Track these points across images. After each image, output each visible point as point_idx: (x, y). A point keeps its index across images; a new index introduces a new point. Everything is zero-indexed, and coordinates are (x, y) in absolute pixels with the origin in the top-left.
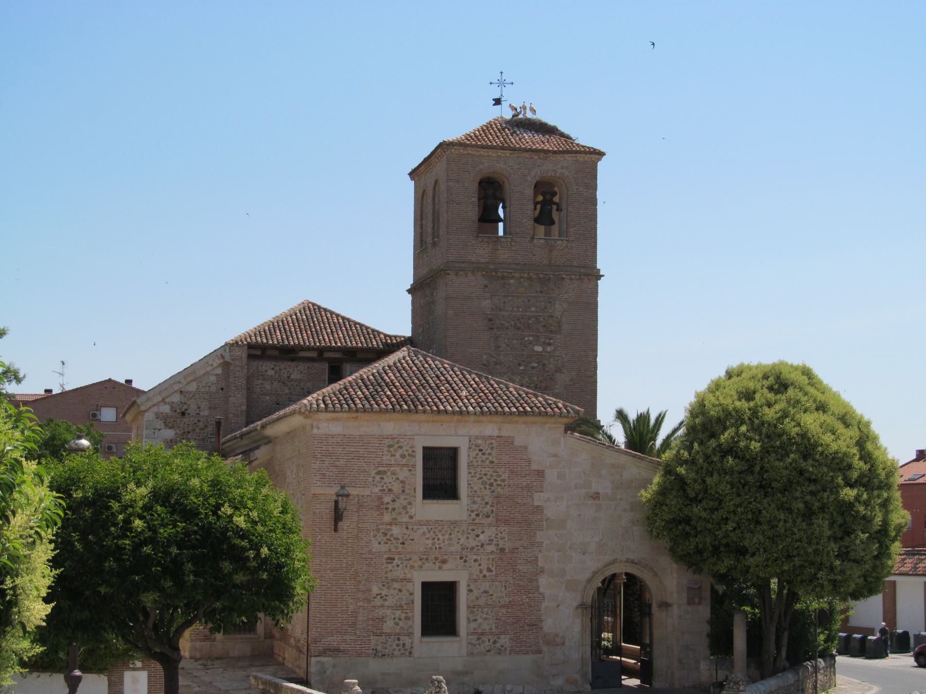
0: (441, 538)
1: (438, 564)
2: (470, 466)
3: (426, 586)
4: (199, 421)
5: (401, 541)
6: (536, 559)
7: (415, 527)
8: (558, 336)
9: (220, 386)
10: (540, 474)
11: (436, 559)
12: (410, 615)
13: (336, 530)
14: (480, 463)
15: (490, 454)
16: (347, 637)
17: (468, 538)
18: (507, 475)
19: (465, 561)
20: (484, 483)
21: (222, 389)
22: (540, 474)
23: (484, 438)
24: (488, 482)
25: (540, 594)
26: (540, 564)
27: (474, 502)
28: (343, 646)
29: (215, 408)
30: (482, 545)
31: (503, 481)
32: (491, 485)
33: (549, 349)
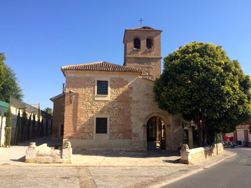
15: (117, 83)
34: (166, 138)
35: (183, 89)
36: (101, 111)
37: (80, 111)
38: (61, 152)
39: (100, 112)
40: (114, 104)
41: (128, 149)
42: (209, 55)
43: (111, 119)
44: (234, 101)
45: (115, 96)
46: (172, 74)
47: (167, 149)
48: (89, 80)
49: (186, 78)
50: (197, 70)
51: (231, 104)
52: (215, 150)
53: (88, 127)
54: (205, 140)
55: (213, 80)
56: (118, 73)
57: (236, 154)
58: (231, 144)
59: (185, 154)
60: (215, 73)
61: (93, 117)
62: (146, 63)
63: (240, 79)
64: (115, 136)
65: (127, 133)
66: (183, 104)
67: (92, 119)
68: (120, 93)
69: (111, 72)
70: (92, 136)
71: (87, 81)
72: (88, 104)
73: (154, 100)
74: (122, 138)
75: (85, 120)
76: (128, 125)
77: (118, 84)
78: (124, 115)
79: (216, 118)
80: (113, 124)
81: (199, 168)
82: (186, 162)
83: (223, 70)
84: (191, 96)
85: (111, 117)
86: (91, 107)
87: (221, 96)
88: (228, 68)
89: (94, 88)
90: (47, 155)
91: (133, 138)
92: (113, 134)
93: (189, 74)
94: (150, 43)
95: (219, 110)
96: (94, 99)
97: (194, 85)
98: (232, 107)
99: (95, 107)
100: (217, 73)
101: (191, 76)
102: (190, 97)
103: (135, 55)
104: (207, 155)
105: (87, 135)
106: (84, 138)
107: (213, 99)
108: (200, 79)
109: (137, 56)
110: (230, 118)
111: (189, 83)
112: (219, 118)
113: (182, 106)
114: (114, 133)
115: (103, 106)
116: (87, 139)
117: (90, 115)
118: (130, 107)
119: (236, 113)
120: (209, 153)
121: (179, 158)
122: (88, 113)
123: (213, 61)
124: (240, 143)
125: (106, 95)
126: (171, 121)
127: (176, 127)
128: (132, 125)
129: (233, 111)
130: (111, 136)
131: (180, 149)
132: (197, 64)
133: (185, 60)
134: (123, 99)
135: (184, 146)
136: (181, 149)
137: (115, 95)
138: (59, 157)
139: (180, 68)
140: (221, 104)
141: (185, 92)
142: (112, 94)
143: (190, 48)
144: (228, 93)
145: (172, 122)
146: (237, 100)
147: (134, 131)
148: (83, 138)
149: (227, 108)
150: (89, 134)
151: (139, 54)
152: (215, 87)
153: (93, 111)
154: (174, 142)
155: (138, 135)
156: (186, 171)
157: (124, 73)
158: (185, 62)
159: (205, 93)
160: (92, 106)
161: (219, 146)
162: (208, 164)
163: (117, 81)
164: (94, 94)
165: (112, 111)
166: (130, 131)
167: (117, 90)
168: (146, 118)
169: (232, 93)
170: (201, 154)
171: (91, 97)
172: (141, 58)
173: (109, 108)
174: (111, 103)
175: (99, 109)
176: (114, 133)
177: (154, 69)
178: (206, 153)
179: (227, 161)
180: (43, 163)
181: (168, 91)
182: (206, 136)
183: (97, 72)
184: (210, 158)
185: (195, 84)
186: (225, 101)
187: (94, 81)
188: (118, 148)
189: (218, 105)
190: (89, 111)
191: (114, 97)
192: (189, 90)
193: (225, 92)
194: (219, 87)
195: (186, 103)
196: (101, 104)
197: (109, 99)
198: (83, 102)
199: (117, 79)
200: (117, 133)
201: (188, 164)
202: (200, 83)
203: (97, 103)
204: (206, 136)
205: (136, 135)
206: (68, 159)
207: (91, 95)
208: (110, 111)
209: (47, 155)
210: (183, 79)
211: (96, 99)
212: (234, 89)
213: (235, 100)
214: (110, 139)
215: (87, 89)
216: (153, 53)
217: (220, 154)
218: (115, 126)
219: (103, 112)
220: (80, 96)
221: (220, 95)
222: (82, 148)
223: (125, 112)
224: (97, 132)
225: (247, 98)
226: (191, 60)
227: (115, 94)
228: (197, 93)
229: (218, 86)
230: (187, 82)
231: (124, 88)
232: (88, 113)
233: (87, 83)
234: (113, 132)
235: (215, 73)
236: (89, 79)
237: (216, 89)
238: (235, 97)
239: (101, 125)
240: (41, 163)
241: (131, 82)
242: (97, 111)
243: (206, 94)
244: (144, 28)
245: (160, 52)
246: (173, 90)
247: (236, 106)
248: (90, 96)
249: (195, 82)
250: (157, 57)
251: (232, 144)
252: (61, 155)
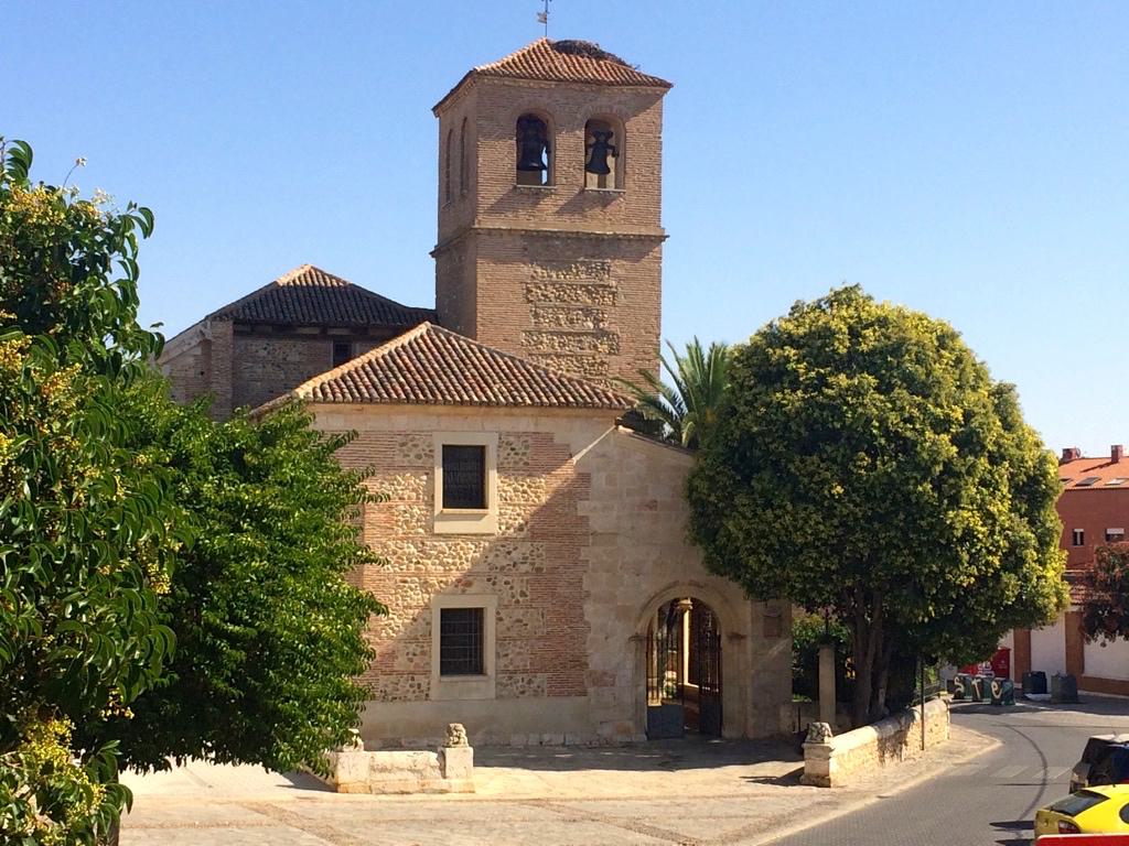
15: (524, 454)
25: (587, 623)
26: (585, 587)
34: (724, 687)
35: (814, 515)
36: (459, 581)
37: (374, 581)
38: (442, 756)
39: (456, 586)
40: (515, 549)
41: (570, 739)
42: (910, 382)
43: (503, 615)
44: (990, 558)
45: (518, 515)
46: (772, 447)
47: (725, 733)
48: (410, 444)
49: (829, 474)
50: (866, 446)
51: (979, 570)
52: (913, 734)
53: (407, 648)
54: (882, 702)
55: (920, 489)
56: (530, 411)
57: (998, 744)
58: (994, 690)
59: (819, 756)
60: (929, 464)
61: (427, 607)
62: (583, 263)
63: (1017, 475)
64: (520, 683)
65: (566, 669)
66: (811, 569)
67: (424, 616)
68: (536, 500)
69: (503, 410)
70: (424, 687)
71: (400, 450)
72: (406, 550)
73: (686, 537)
74: (546, 694)
75: (397, 620)
76: (572, 638)
77: (533, 458)
78: (553, 595)
79: (923, 621)
80: (509, 634)
81: (864, 795)
82: (822, 781)
83: (958, 447)
84: (842, 542)
85: (502, 606)
86: (419, 563)
87: (944, 545)
88: (975, 440)
89: (431, 479)
90: (402, 769)
91: (591, 690)
92: (510, 678)
93: (839, 460)
94: (602, 145)
95: (935, 592)
96: (429, 529)
97: (853, 502)
98: (982, 579)
99: (437, 562)
100: (935, 462)
101: (844, 467)
102: (835, 541)
103: (524, 220)
104: (887, 755)
105: (405, 685)
106: (391, 694)
107: (917, 555)
108: (876, 482)
109: (532, 226)
110: (972, 621)
111: (839, 494)
112: (938, 620)
113: (806, 575)
114: (515, 672)
115: (470, 556)
116: (405, 699)
117: (416, 597)
118: (581, 558)
119: (995, 602)
120: (892, 745)
121: (793, 767)
122: (406, 592)
123: (922, 408)
124: (1037, 682)
125: (481, 511)
126: (749, 618)
127: (766, 641)
128: (591, 635)
129: (982, 594)
130: (501, 684)
131: (802, 736)
132: (869, 421)
133: (825, 401)
134: (554, 526)
135: (816, 727)
136: (809, 737)
137: (518, 511)
138: (437, 773)
139: (802, 430)
140: (942, 571)
141: (822, 527)
142: (508, 501)
143: (838, 339)
144: (969, 534)
145: (752, 622)
146: (1000, 553)
147: (595, 661)
148: (390, 697)
149: (965, 585)
150: (413, 679)
151: (548, 217)
152: (928, 512)
153: (426, 582)
154: (755, 706)
155: (614, 676)
156: (833, 804)
157: (557, 411)
158: (822, 407)
159: (892, 534)
160: (422, 558)
161: (930, 714)
162: (889, 785)
163: (527, 447)
164: (433, 505)
165: (506, 579)
166: (580, 663)
167: (525, 488)
168: (645, 607)
169: (983, 533)
170: (866, 751)
171: (418, 520)
172: (558, 238)
173: (498, 561)
174: (503, 546)
175: (451, 570)
176: (515, 672)
177: (622, 300)
178: (883, 745)
179: (952, 774)
180: (391, 793)
181: (755, 515)
182: (883, 683)
183: (441, 409)
184: (896, 764)
185: (858, 500)
186: (956, 561)
187: (428, 446)
188: (532, 735)
189: (933, 577)
190: (412, 582)
191: (515, 519)
192: (836, 522)
193: (959, 533)
194: (939, 513)
195: (819, 567)
196: (462, 549)
197: (495, 530)
198: (384, 540)
199: (528, 438)
200: (525, 671)
201: (829, 787)
202: (875, 497)
203: (443, 545)
204: (883, 683)
205: (601, 679)
206: (464, 781)
207: (416, 510)
208: (499, 578)
209: (402, 769)
210: (816, 478)
211: (440, 527)
212: (989, 517)
213: (995, 554)
214: (499, 697)
215: (399, 484)
216: (619, 207)
217: (935, 749)
218: (519, 642)
219: (469, 584)
220: (372, 515)
221: (943, 541)
222: (389, 735)
223: (560, 584)
224: (446, 669)
225: (1037, 545)
226: (847, 403)
227: (519, 505)
228: (863, 529)
229: (936, 512)
230: (829, 491)
231: (555, 476)
232: (406, 592)
233: (400, 458)
234: (511, 668)
235: (929, 464)
236: (406, 440)
237: (929, 519)
238: (992, 545)
239: (460, 638)
240: (384, 793)
241: (585, 451)
242: (444, 579)
243: (895, 537)
244: (565, 47)
245: (659, 202)
246: (777, 517)
247: (997, 576)
248: (412, 516)
249: (855, 490)
250: (644, 231)
251: (997, 693)
252: (443, 768)
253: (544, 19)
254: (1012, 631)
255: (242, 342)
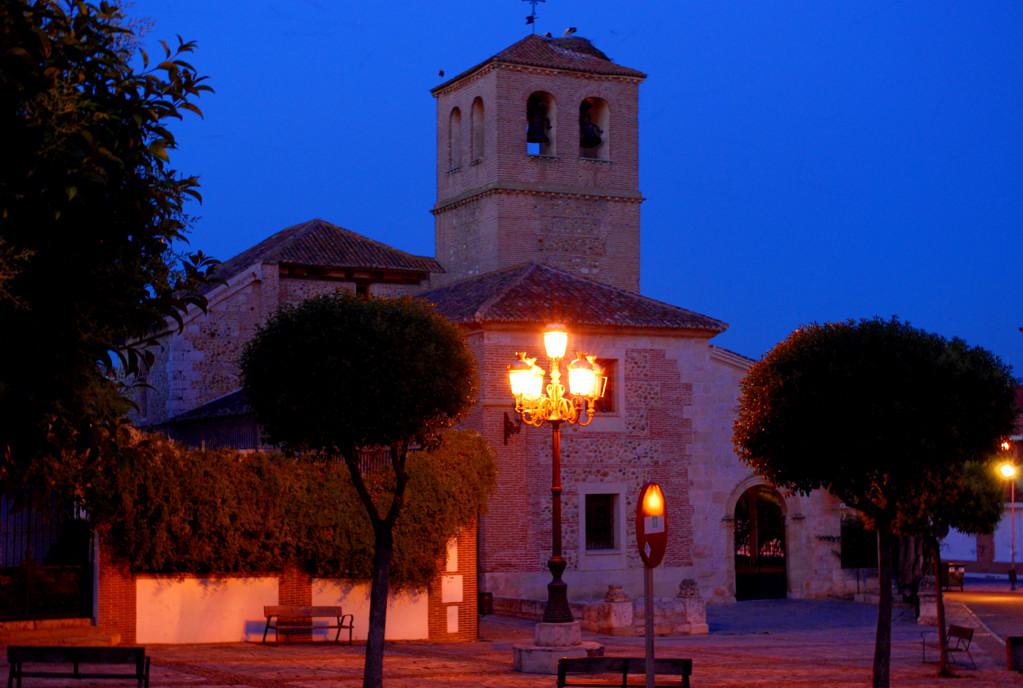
0: (603, 451)
1: (600, 477)
2: (627, 378)
3: (589, 498)
4: (229, 343)
5: (566, 454)
6: (686, 472)
7: (580, 440)
8: (603, 259)
9: (250, 307)
10: (688, 387)
11: (598, 471)
12: (575, 528)
13: (506, 443)
14: (635, 376)
15: (644, 367)
16: (518, 552)
17: (626, 451)
18: (659, 388)
19: (624, 474)
20: (639, 396)
21: (252, 309)
22: (688, 387)
23: (639, 351)
24: (644, 395)
25: (691, 506)
26: (690, 477)
27: (631, 415)
28: (514, 561)
29: (246, 329)
30: (639, 458)
31: (656, 394)
32: (646, 398)
33: (595, 271)
253: (530, 20)
254: (893, 581)
255: (283, 283)
